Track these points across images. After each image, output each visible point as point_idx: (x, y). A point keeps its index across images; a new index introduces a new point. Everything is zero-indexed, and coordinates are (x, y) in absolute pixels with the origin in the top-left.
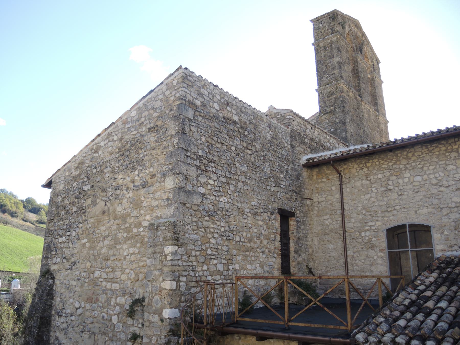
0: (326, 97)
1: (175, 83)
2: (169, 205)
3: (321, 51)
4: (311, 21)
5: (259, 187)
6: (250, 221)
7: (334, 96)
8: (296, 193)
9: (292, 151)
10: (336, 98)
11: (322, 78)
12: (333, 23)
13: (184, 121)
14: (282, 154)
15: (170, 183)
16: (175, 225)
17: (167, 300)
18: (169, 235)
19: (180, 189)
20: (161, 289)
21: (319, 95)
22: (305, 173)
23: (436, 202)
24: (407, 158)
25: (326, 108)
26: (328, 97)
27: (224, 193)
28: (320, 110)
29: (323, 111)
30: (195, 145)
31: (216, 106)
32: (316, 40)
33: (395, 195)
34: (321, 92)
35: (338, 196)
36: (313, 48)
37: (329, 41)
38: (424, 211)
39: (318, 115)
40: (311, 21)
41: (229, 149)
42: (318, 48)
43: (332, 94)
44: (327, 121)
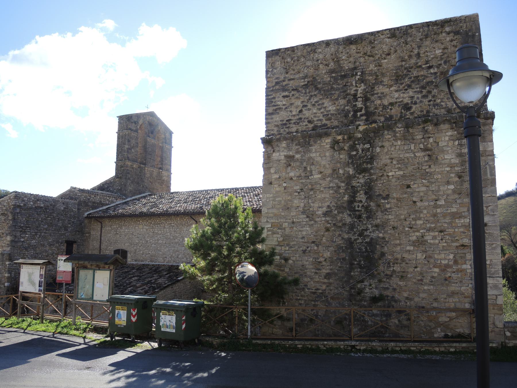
1: (12, 198)
2: (8, 247)
4: (118, 117)
5: (53, 233)
6: (48, 248)
8: (78, 231)
9: (78, 212)
10: (123, 170)
13: (15, 214)
14: (71, 215)
15: (9, 238)
16: (10, 254)
17: (6, 280)
18: (8, 258)
19: (12, 241)
20: (5, 276)
22: (86, 221)
23: (130, 241)
24: (125, 221)
27: (34, 239)
30: (20, 223)
31: (32, 203)
32: (119, 130)
33: (118, 236)
35: (100, 233)
38: (127, 244)
40: (118, 117)
41: (37, 220)
43: (122, 167)
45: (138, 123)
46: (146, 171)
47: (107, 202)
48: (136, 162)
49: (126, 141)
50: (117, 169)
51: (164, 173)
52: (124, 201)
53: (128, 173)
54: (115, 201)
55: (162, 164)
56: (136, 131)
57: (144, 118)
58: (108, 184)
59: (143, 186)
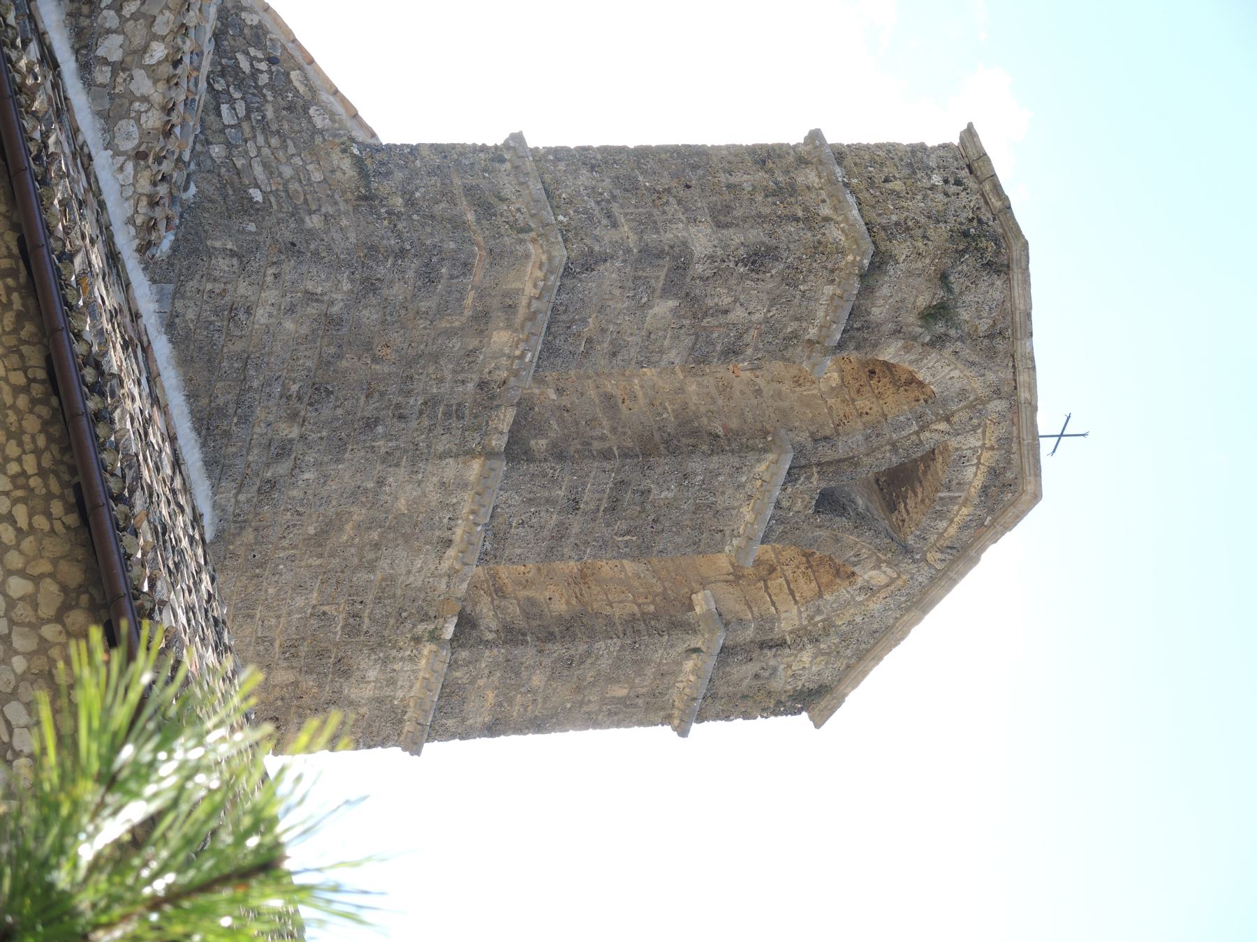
0: (471, 181)
3: (771, 172)
4: (970, 134)
7: (470, 217)
10: (457, 224)
11: (592, 168)
12: (939, 233)
21: (484, 148)
25: (399, 175)
26: (469, 190)
28: (390, 148)
29: (382, 164)
32: (840, 154)
34: (502, 160)
36: (794, 136)
37: (826, 211)
39: (360, 136)
40: (970, 134)
42: (791, 159)
43: (486, 209)
44: (317, 176)
45: (938, 342)
46: (450, 468)
47: (111, 48)
48: (549, 351)
49: (756, 235)
50: (448, 158)
51: (419, 671)
52: (126, 243)
53: (428, 276)
54: (129, 136)
55: (511, 635)
56: (858, 330)
57: (975, 407)
58: (281, 84)
59: (284, 450)
